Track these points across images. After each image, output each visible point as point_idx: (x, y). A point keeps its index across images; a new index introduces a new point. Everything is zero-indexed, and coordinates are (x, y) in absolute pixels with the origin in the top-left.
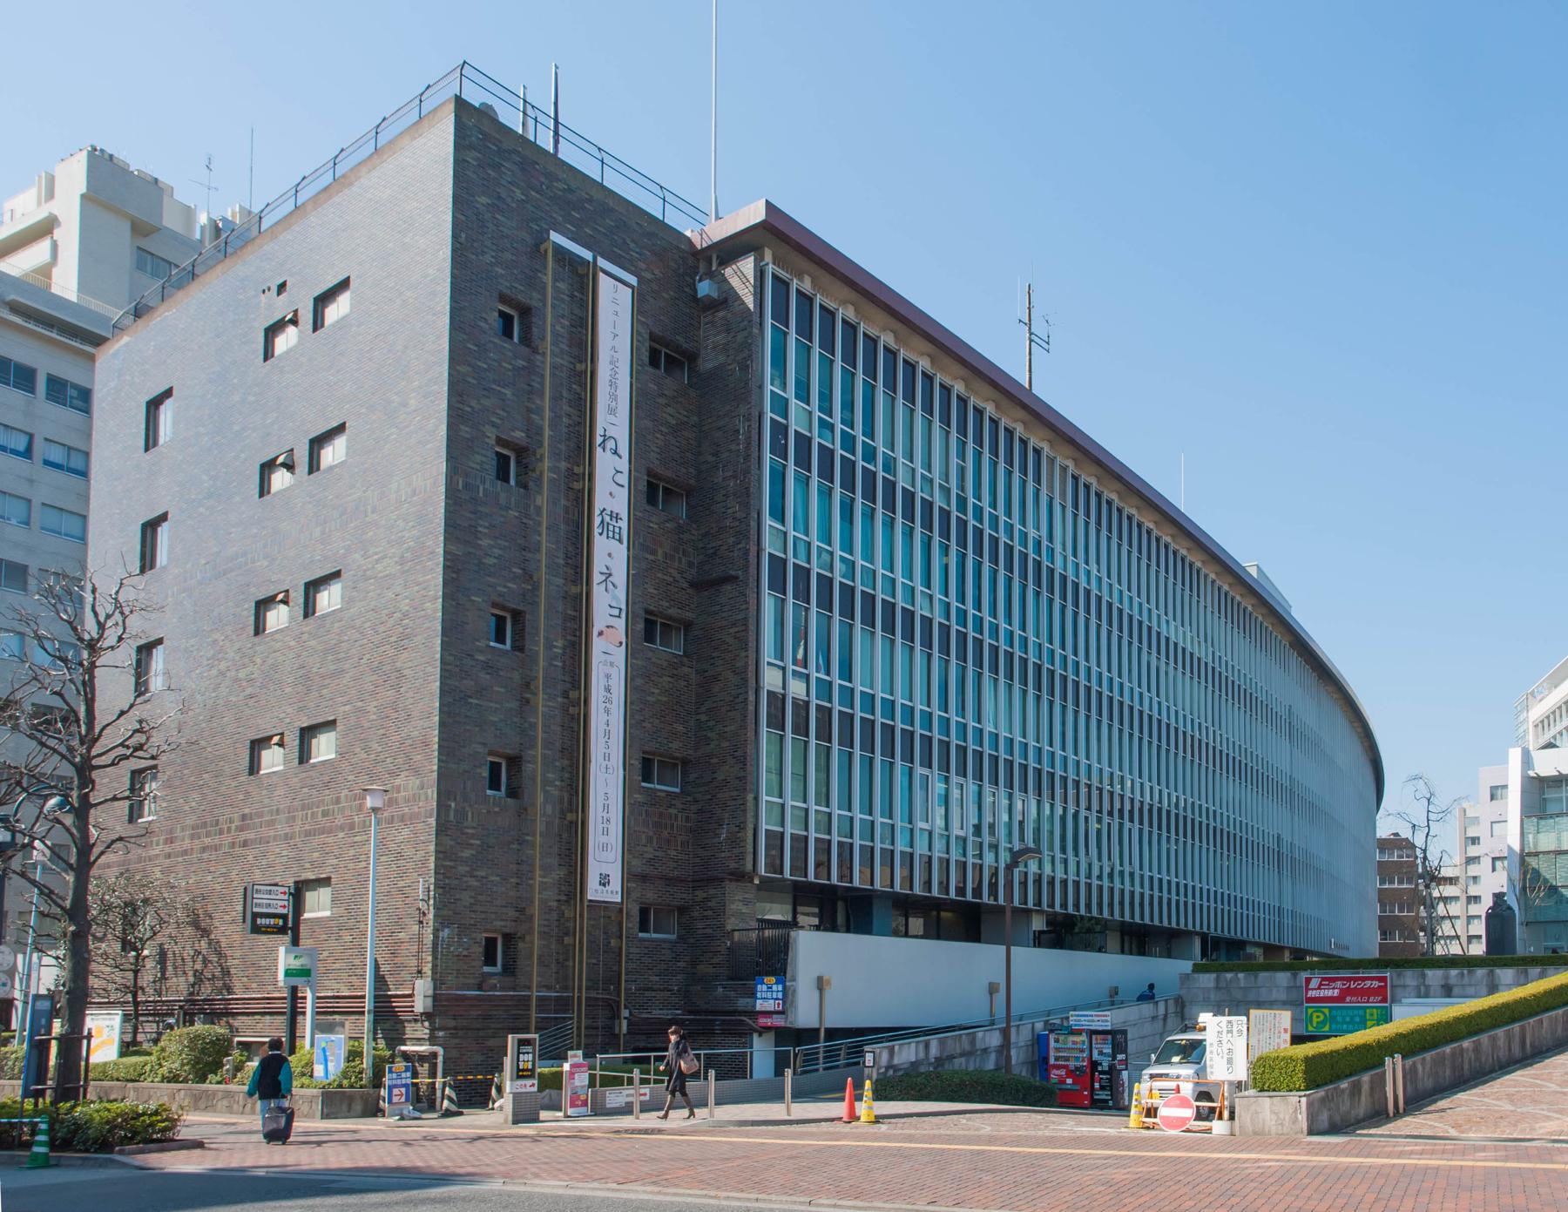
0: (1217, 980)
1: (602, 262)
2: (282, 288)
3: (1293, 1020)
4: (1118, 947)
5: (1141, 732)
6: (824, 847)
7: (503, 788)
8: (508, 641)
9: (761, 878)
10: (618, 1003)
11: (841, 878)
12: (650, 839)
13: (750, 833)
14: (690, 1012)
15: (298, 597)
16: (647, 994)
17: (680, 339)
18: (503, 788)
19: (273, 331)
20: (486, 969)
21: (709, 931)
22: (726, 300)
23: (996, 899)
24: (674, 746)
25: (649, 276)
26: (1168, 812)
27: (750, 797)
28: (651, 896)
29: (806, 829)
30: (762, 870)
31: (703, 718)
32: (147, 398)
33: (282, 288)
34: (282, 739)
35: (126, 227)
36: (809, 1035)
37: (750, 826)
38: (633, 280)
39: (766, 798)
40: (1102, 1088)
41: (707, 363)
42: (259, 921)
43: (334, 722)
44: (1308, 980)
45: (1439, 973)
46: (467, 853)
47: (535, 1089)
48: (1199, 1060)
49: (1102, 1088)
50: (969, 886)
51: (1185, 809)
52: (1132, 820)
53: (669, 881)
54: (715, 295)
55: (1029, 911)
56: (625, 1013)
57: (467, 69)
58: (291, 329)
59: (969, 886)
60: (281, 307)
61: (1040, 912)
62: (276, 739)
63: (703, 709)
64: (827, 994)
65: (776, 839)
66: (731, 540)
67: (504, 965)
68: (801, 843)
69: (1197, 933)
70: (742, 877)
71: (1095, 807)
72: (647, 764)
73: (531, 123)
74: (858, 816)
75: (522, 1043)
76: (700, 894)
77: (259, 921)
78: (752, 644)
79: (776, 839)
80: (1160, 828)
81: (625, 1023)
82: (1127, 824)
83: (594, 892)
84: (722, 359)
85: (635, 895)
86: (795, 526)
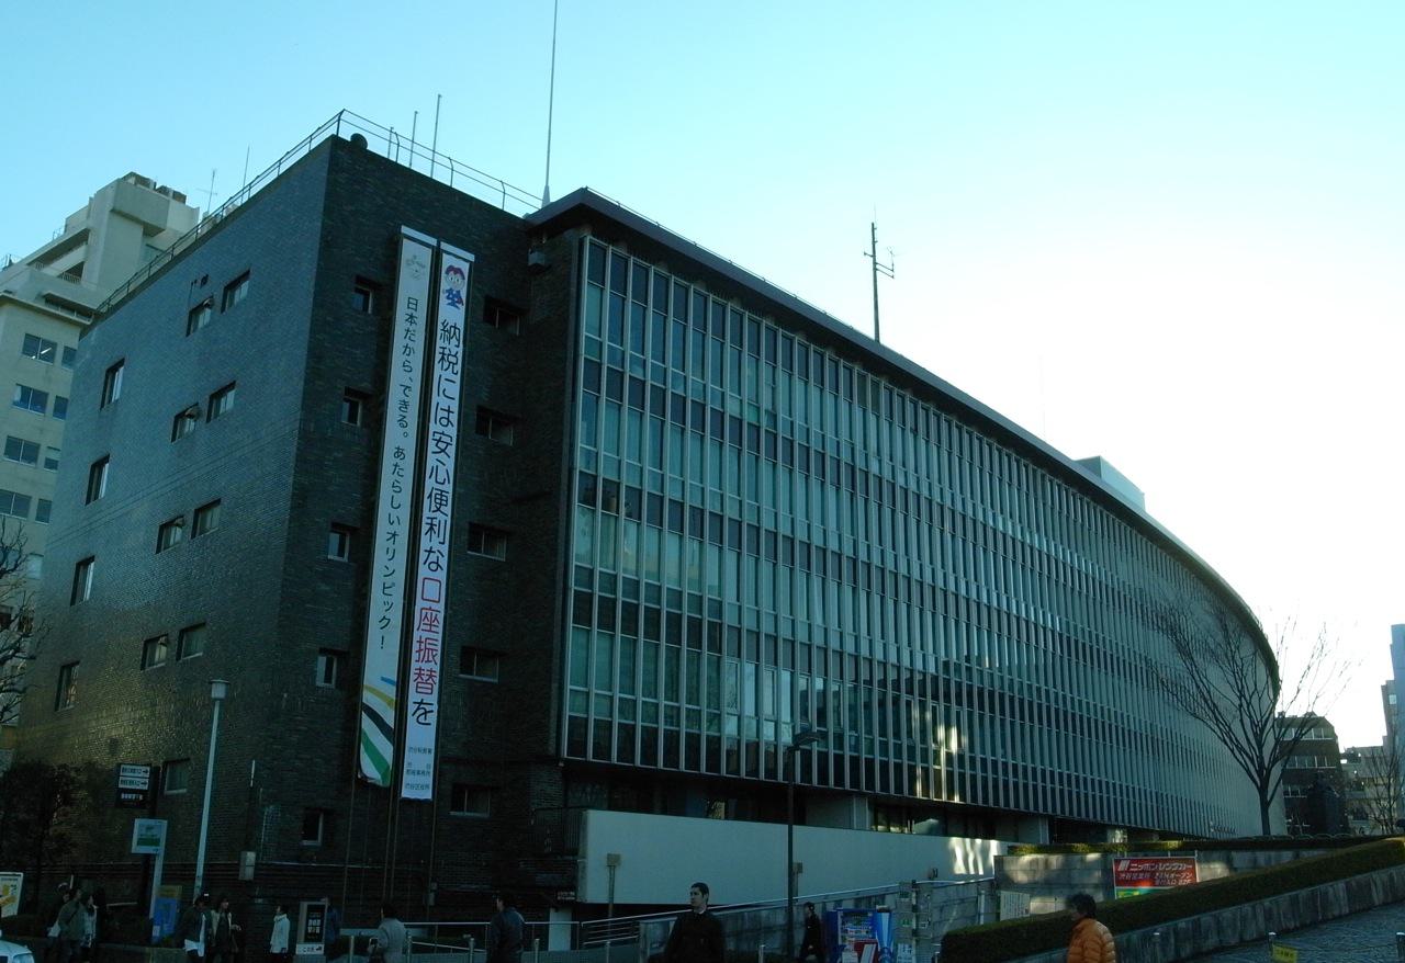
1: (444, 246)
2: (205, 280)
6: (628, 732)
8: (346, 555)
9: (566, 761)
11: (882, 790)
13: (553, 721)
15: (190, 519)
19: (196, 312)
22: (550, 266)
26: (1002, 696)
27: (555, 686)
29: (611, 716)
30: (565, 754)
32: (107, 367)
33: (205, 280)
34: (167, 640)
35: (139, 231)
36: (599, 910)
37: (554, 712)
38: (471, 257)
42: (123, 796)
43: (204, 624)
45: (1247, 855)
46: (295, 738)
47: (322, 952)
48: (830, 918)
51: (1021, 691)
52: (959, 703)
54: (542, 262)
55: (849, 794)
58: (208, 311)
60: (200, 295)
61: (861, 795)
62: (162, 640)
64: (619, 873)
65: (579, 725)
67: (323, 838)
68: (604, 727)
72: (467, 653)
73: (394, 147)
74: (663, 702)
75: (311, 909)
77: (123, 796)
78: (561, 549)
79: (579, 725)
80: (1022, 718)
81: (432, 895)
82: (954, 708)
86: (605, 441)
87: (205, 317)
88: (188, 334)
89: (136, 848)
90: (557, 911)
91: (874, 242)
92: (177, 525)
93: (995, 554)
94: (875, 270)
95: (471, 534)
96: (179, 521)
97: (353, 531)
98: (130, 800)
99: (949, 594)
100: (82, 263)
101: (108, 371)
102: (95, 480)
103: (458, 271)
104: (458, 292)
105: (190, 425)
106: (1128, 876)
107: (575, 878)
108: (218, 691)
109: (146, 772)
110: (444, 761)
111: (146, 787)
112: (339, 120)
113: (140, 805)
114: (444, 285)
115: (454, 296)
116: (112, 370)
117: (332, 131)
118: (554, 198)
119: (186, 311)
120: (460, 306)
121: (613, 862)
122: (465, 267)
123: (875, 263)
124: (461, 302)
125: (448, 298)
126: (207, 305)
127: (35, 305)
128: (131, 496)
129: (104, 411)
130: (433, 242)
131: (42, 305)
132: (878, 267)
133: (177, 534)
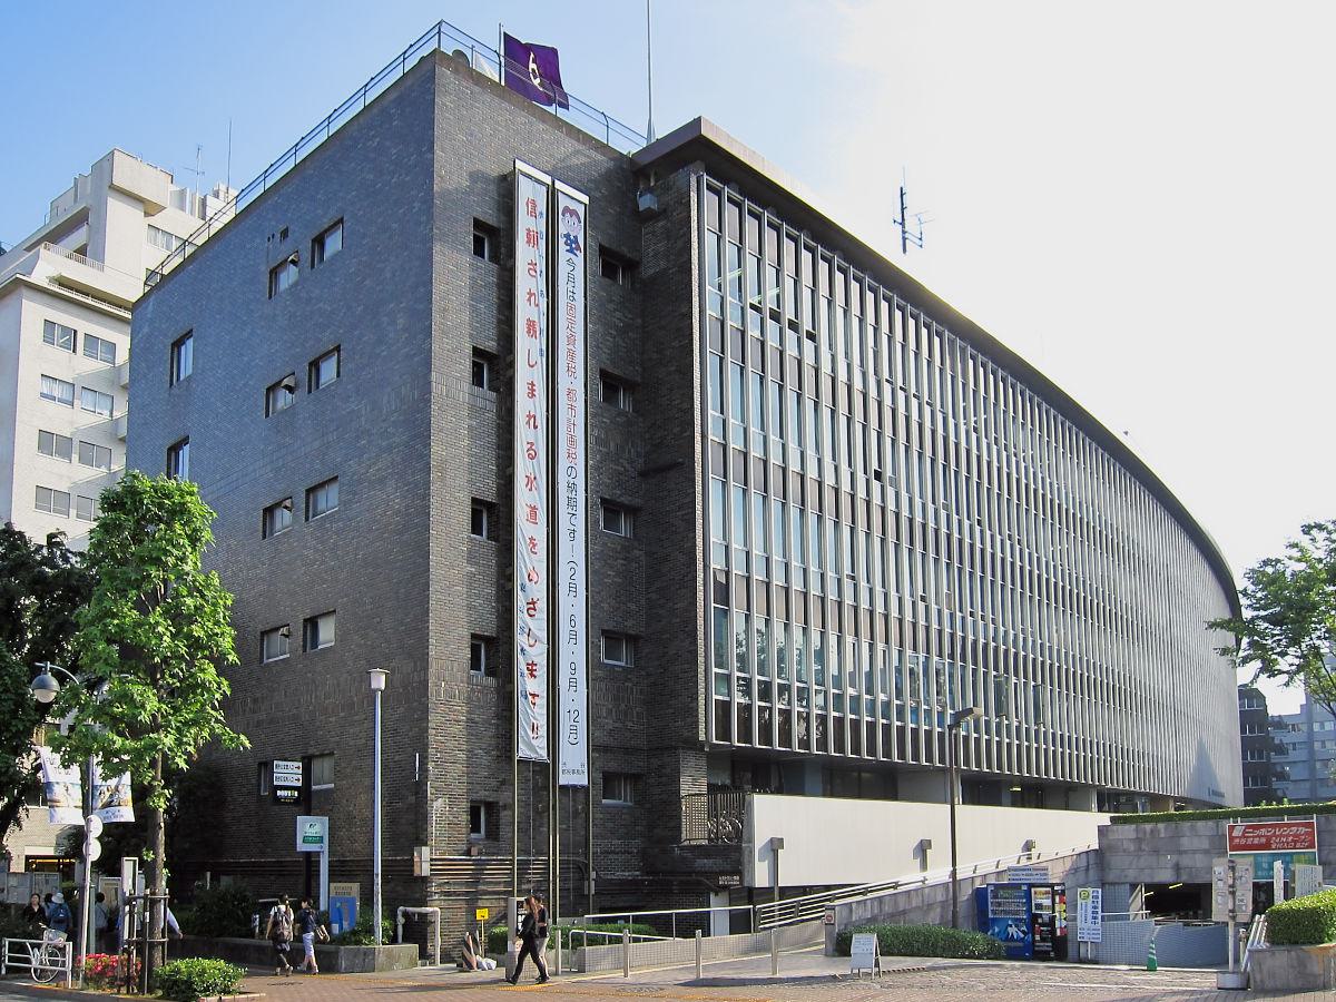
0: (1137, 831)
1: (559, 185)
2: (285, 234)
3: (413, 871)
4: (1009, 801)
5: (1003, 579)
7: (483, 668)
10: (587, 865)
12: (610, 712)
14: (648, 874)
16: (610, 856)
17: (625, 250)
18: (483, 668)
20: (473, 836)
21: (664, 797)
22: (665, 210)
23: (770, 743)
24: (629, 623)
25: (598, 195)
28: (613, 766)
31: (654, 596)
33: (285, 234)
38: (586, 199)
39: (715, 670)
40: (1043, 940)
41: (649, 270)
42: (279, 793)
44: (1232, 828)
49: (1043, 940)
50: (814, 736)
52: (1016, 674)
53: (627, 751)
54: (655, 207)
56: (593, 875)
57: (444, 26)
59: (814, 736)
60: (285, 250)
63: (654, 589)
66: (676, 430)
69: (1094, 786)
70: (695, 746)
71: (947, 651)
76: (655, 762)
77: (279, 793)
80: (975, 663)
81: (593, 883)
83: (523, 751)
84: (663, 264)
85: (597, 764)
87: (289, 277)
88: (270, 297)
89: (301, 847)
90: (716, 895)
91: (903, 209)
92: (286, 507)
93: (897, 546)
94: (904, 239)
95: (608, 508)
96: (288, 503)
97: (490, 506)
98: (286, 798)
99: (774, 589)
100: (86, 245)
101: (173, 345)
102: (173, 463)
103: (573, 213)
104: (576, 237)
105: (283, 399)
106: (1243, 841)
107: (739, 862)
108: (379, 681)
109: (298, 768)
110: (596, 748)
111: (300, 784)
112: (439, 33)
113: (296, 802)
114: (562, 230)
115: (572, 242)
116: (178, 344)
117: (433, 45)
118: (660, 134)
119: (265, 269)
120: (578, 253)
121: (775, 845)
122: (581, 210)
123: (904, 232)
124: (578, 248)
125: (566, 243)
126: (293, 262)
127: (51, 288)
128: (222, 478)
129: (175, 391)
130: (548, 180)
131: (56, 289)
132: (907, 235)
133: (284, 518)
